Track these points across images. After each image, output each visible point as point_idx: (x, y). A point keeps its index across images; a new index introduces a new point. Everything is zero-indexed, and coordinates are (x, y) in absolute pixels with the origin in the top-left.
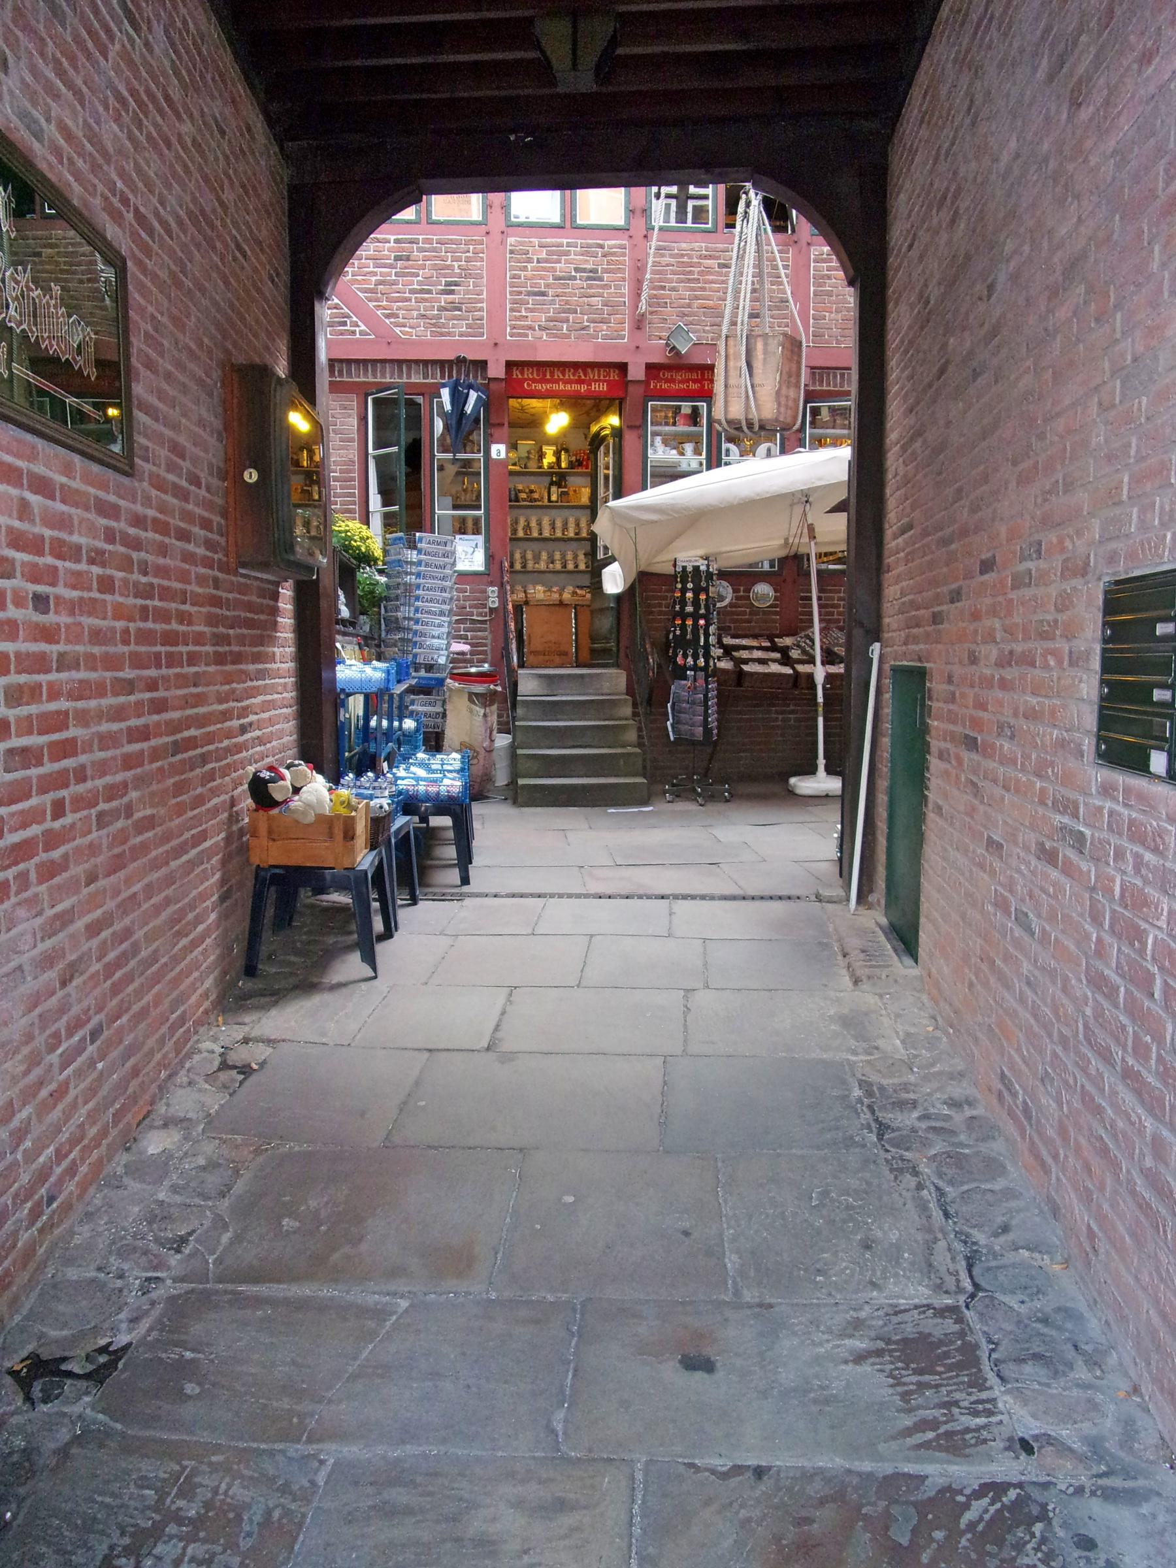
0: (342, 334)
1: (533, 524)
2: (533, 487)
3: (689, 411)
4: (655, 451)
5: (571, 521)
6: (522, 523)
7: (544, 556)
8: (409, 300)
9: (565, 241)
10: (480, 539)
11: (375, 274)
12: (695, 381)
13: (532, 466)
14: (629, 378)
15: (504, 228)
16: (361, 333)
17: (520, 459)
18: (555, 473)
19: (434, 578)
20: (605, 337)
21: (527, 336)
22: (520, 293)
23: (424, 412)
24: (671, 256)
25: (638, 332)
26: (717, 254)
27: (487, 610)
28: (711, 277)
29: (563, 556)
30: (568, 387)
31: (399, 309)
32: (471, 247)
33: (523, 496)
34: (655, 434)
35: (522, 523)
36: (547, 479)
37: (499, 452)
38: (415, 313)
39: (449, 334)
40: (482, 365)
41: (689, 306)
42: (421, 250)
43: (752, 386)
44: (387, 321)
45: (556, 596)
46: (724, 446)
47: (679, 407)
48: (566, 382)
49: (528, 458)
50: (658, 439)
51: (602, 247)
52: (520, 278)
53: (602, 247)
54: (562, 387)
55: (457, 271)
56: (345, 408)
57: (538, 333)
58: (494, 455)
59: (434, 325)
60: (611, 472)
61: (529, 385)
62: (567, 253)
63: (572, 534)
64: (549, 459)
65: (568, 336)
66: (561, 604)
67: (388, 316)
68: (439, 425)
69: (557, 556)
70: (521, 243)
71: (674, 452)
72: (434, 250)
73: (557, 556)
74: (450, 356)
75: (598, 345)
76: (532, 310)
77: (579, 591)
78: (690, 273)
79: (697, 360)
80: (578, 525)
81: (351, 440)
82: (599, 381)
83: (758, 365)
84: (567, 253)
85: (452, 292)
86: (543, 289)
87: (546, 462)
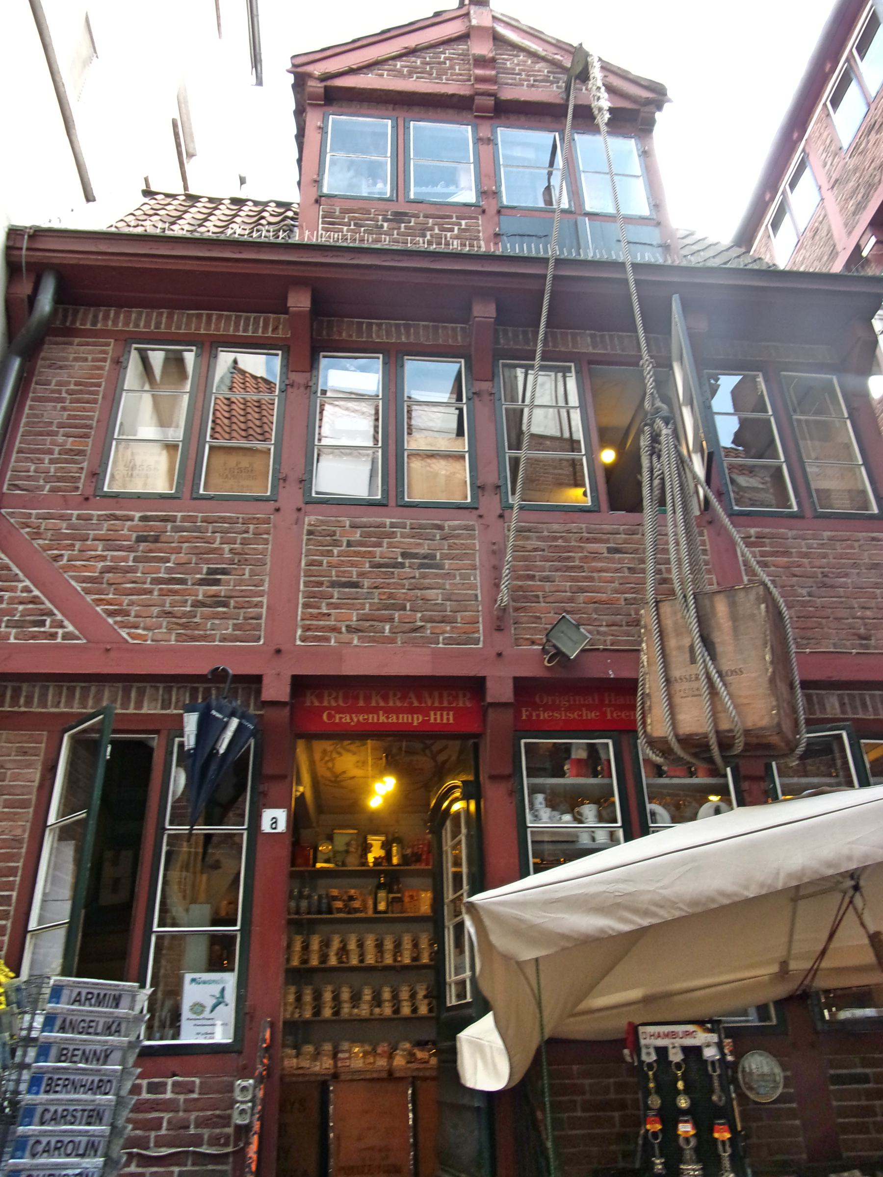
0: (33, 638)
1: (352, 945)
2: (352, 892)
3: (582, 754)
4: (537, 818)
5: (407, 941)
6: (336, 944)
7: (367, 995)
8: (150, 592)
9: (388, 521)
10: (230, 980)
11: (103, 558)
12: (590, 708)
13: (352, 863)
14: (489, 699)
15: (301, 504)
16: (66, 636)
17: (335, 853)
18: (382, 872)
19: (76, 1087)
20: (449, 641)
21: (328, 639)
22: (321, 584)
23: (158, 758)
24: (539, 539)
25: (497, 635)
26: (605, 537)
27: (230, 1130)
28: (600, 565)
29: (395, 997)
30: (393, 719)
31: (131, 603)
32: (252, 526)
33: (339, 904)
34: (534, 790)
35: (336, 944)
36: (371, 882)
37: (275, 821)
38: (155, 610)
39: (204, 638)
40: (254, 681)
41: (571, 600)
42: (176, 529)
43: (720, 675)
44: (110, 621)
45: (382, 1062)
46: (649, 807)
47: (567, 748)
48: (388, 711)
49: (347, 852)
50: (540, 798)
51: (440, 528)
52: (320, 564)
53: (440, 528)
54: (382, 719)
55: (227, 555)
56: (25, 753)
57: (345, 636)
58: (266, 826)
59: (184, 626)
60: (464, 870)
61: (330, 717)
62: (392, 535)
63: (407, 961)
64: (375, 853)
65: (392, 641)
66: (391, 1076)
67: (111, 614)
68: (179, 780)
69: (387, 995)
70: (323, 522)
71: (567, 817)
72: (198, 530)
73: (387, 995)
74: (204, 669)
75: (436, 654)
76: (336, 606)
77: (420, 1054)
78: (568, 559)
79: (596, 669)
80: (416, 945)
81: (24, 804)
82: (442, 709)
83: (723, 636)
84: (392, 535)
85: (217, 582)
86: (355, 579)
87: (371, 858)
